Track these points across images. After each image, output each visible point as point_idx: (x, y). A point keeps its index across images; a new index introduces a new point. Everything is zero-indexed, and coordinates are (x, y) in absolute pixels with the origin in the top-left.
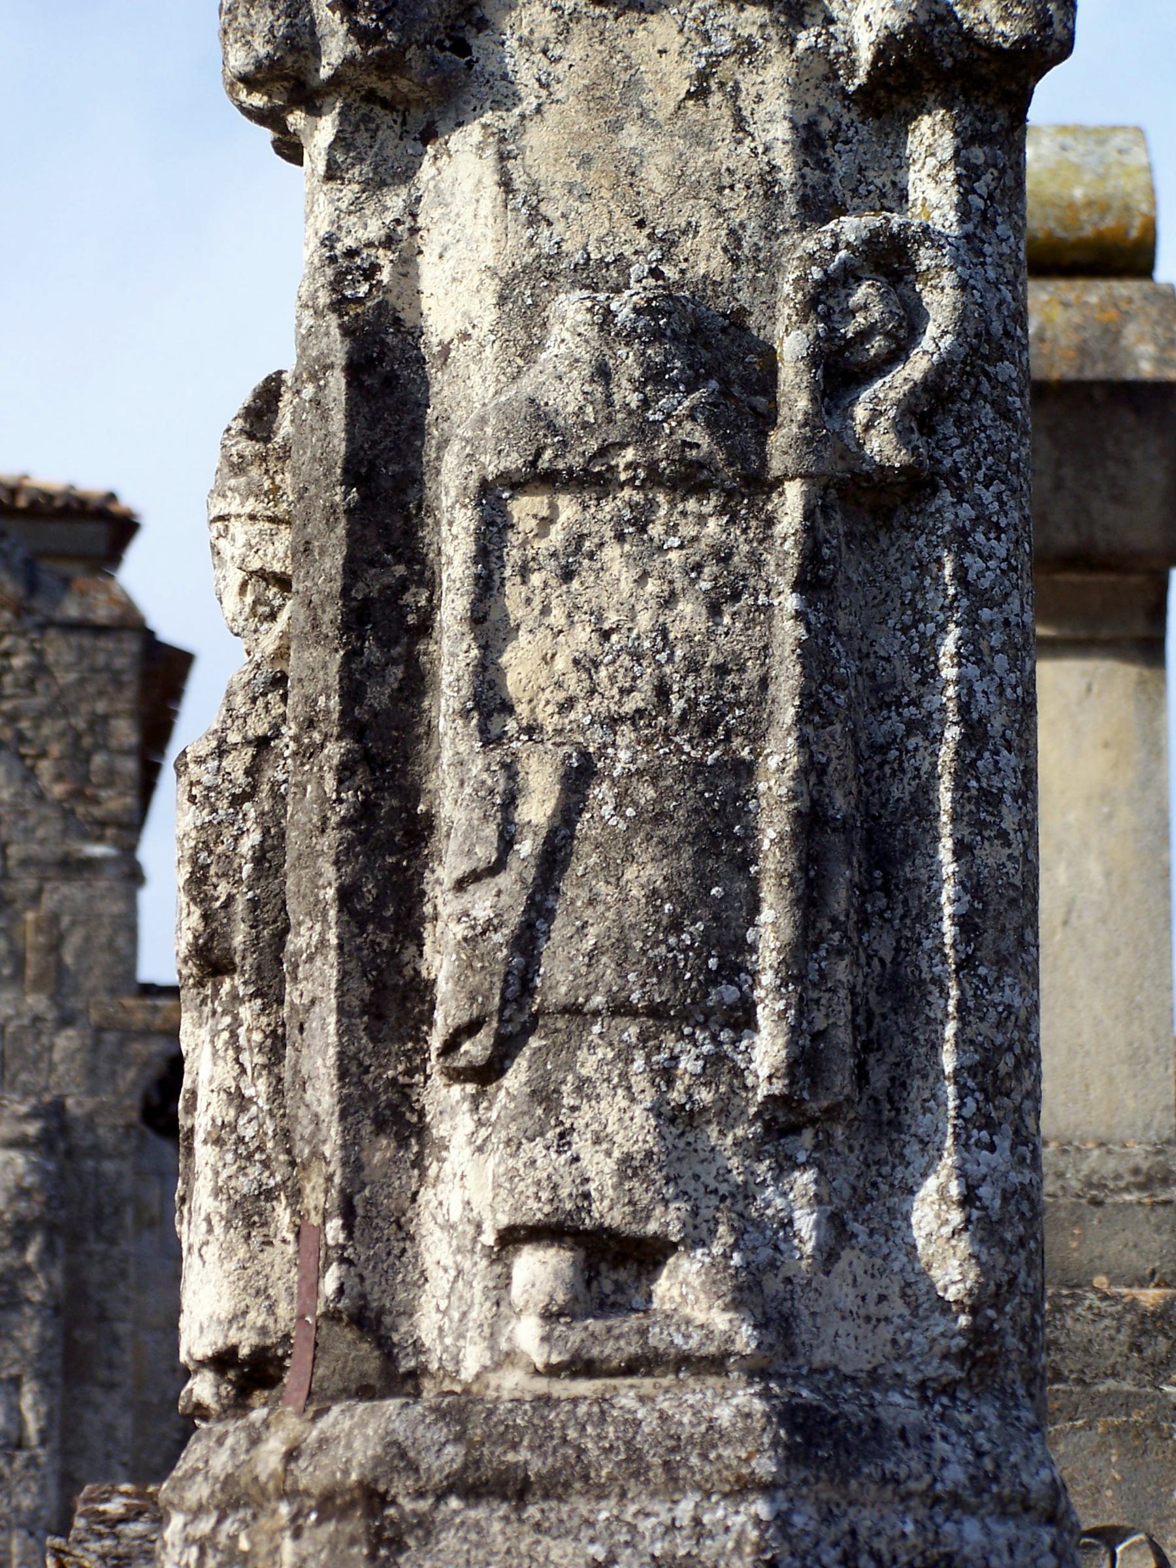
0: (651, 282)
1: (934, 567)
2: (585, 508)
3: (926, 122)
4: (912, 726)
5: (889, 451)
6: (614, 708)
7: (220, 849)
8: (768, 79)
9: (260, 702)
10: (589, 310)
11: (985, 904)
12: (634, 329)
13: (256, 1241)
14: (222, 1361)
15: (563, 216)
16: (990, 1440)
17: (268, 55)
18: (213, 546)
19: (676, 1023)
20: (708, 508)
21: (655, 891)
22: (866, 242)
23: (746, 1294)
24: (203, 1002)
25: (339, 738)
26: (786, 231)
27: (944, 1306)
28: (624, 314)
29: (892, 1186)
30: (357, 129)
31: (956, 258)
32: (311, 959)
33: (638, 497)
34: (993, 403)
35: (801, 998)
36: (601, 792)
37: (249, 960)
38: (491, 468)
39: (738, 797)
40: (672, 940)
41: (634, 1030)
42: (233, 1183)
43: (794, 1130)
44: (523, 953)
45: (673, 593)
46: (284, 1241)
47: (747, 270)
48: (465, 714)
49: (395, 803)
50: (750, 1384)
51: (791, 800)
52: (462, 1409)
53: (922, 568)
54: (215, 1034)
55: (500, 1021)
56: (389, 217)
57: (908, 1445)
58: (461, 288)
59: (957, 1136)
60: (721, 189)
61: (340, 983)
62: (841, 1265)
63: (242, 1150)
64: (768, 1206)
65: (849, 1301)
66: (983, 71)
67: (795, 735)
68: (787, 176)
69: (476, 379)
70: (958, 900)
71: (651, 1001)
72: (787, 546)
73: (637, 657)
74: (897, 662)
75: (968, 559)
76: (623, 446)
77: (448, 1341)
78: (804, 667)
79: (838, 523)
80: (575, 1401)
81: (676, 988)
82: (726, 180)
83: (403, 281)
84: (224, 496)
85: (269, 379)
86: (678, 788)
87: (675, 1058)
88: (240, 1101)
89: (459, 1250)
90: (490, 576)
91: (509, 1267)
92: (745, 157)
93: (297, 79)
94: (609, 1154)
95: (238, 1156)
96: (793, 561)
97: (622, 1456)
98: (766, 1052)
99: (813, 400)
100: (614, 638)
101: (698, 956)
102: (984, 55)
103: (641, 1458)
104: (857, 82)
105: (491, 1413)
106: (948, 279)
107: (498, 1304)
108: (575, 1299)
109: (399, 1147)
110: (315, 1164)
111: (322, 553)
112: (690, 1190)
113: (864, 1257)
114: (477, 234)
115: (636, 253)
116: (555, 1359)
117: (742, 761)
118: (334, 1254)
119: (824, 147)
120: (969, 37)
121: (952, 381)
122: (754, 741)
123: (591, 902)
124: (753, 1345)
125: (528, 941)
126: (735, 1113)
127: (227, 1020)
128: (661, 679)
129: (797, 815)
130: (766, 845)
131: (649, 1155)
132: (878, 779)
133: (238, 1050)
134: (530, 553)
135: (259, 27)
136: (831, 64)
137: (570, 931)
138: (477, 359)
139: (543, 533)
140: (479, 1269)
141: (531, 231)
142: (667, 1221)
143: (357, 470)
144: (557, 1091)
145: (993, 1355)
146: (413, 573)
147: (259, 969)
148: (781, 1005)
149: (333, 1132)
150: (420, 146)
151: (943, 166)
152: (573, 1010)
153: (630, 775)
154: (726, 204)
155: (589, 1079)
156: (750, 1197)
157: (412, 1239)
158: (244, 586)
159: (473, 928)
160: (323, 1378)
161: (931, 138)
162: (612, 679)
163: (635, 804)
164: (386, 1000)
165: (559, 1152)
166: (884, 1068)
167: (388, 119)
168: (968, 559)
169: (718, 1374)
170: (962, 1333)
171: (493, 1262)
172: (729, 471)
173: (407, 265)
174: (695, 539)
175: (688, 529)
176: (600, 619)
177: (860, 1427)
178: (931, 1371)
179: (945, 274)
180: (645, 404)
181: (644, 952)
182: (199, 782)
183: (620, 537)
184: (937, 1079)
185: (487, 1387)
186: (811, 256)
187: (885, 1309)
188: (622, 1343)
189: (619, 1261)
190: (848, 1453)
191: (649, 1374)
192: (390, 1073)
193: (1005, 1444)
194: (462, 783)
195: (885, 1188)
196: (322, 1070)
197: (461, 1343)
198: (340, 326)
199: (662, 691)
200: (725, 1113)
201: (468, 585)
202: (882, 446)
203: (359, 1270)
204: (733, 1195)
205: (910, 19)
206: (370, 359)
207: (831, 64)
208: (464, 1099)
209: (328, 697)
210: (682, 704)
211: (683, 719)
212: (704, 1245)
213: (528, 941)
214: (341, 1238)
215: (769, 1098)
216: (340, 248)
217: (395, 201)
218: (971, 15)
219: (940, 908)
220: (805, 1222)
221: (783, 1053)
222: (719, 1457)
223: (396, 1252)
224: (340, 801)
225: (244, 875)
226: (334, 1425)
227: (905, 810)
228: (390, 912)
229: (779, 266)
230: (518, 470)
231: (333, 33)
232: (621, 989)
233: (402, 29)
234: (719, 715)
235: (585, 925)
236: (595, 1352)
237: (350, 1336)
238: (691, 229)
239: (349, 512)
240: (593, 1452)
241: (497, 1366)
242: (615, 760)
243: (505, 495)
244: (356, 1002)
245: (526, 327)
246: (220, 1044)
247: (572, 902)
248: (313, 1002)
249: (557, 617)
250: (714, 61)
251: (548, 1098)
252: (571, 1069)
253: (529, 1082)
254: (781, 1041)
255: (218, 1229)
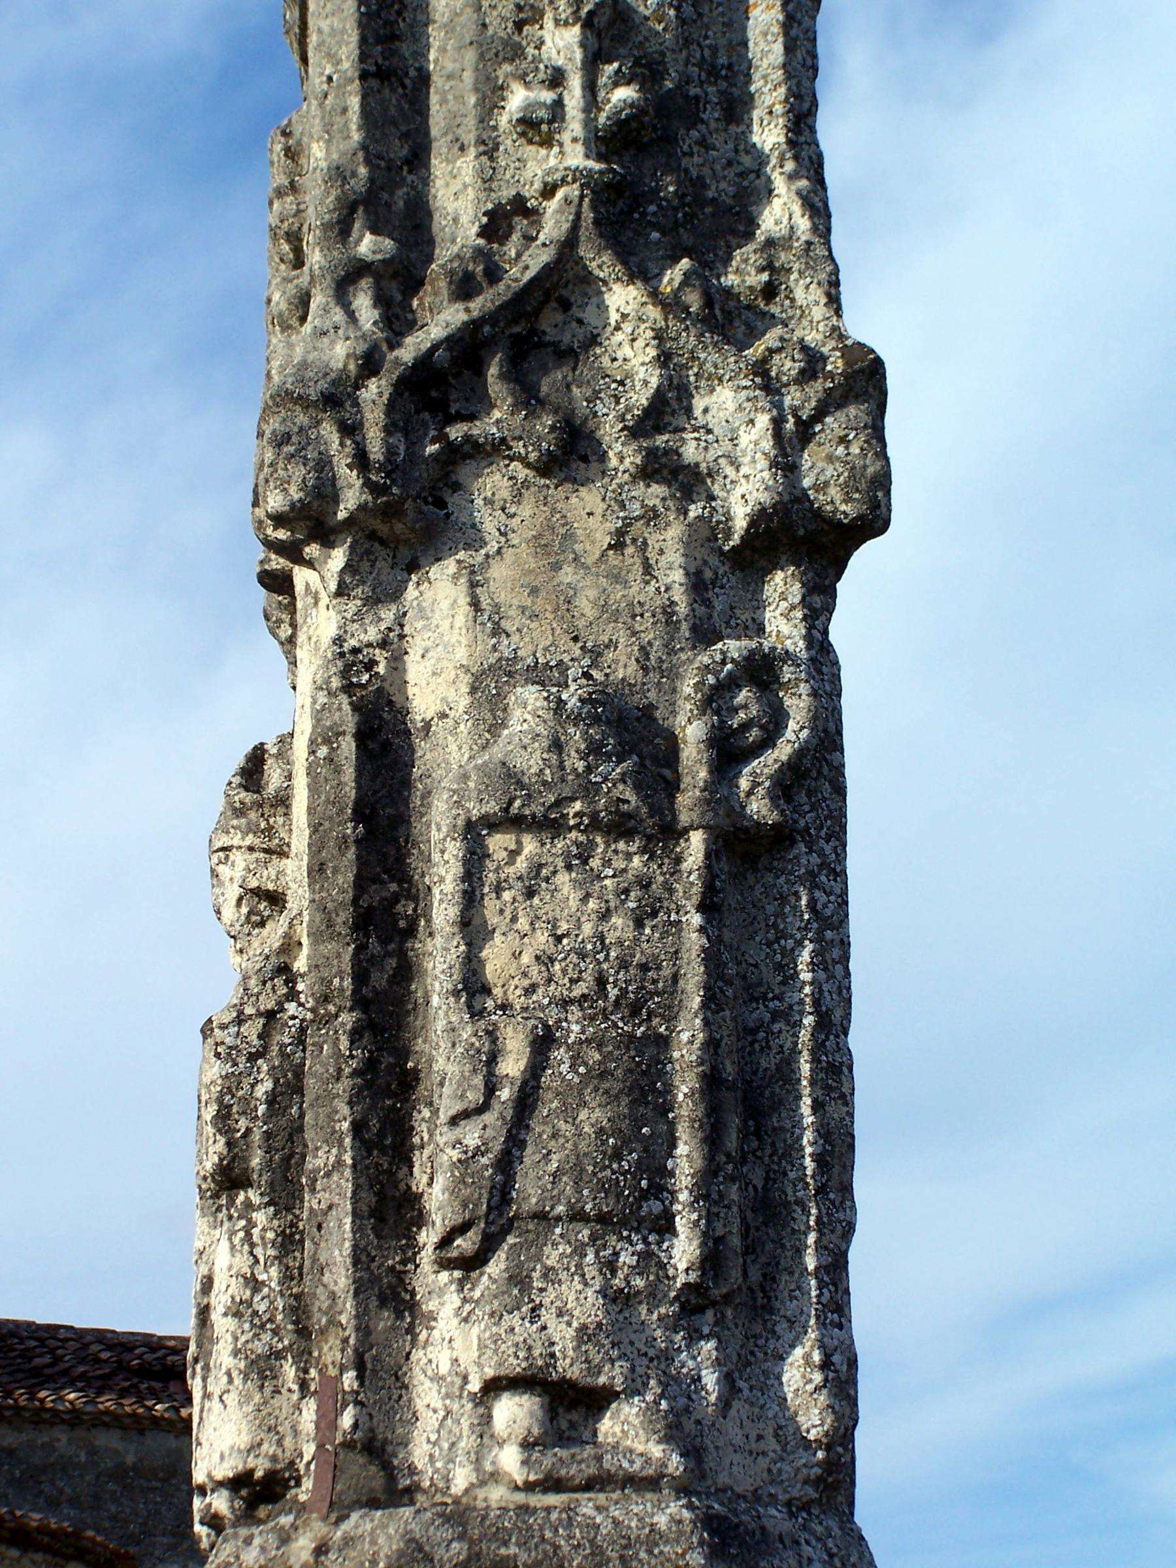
0: (584, 681)
1: (792, 899)
2: (543, 844)
3: (779, 576)
4: (776, 1015)
5: (764, 812)
6: (565, 993)
7: (241, 1093)
8: (668, 538)
9: (269, 985)
10: (546, 699)
11: (833, 1146)
12: (580, 714)
13: (268, 1390)
14: (238, 1483)
15: (518, 630)
16: (836, 1545)
17: (300, 500)
18: (212, 871)
19: (617, 1228)
20: (633, 848)
21: (602, 1129)
22: (746, 659)
23: (674, 1431)
24: (219, 1209)
25: (351, 1010)
26: (682, 649)
27: (806, 1444)
28: (572, 703)
29: (766, 1354)
30: (361, 559)
31: (809, 673)
32: (328, 1175)
33: (582, 838)
34: (830, 782)
35: (708, 1211)
36: (559, 1054)
37: (264, 1178)
38: (475, 812)
39: (659, 1062)
40: (615, 1166)
41: (586, 1232)
42: (250, 1346)
43: (700, 1310)
44: (503, 1173)
45: (608, 910)
46: (290, 1390)
47: (654, 677)
48: (456, 993)
49: (391, 1060)
50: (678, 1499)
51: (699, 1065)
52: (462, 1515)
53: (783, 899)
54: (232, 1233)
55: (486, 1223)
56: (383, 626)
57: (785, 1547)
58: (440, 680)
59: (818, 1317)
60: (634, 616)
61: (354, 1193)
62: (733, 1412)
63: (256, 1321)
64: (682, 1367)
65: (738, 1440)
66: (824, 540)
67: (701, 1017)
68: (682, 609)
69: (453, 747)
70: (815, 1143)
71: (600, 1210)
72: (692, 878)
73: (582, 955)
74: (763, 968)
75: (817, 894)
76: (573, 799)
77: (439, 1465)
78: (706, 967)
79: (724, 865)
80: (548, 1510)
81: (618, 1202)
82: (638, 610)
83: (395, 673)
84: (228, 833)
85: (255, 748)
86: (616, 1053)
87: (616, 1254)
88: (254, 1284)
89: (447, 1396)
90: (473, 891)
91: (489, 1409)
92: (652, 594)
93: (317, 520)
94: (569, 1324)
95: (253, 1326)
96: (697, 890)
97: (588, 1551)
98: (683, 1251)
99: (711, 772)
100: (565, 941)
101: (634, 1178)
102: (826, 527)
103: (602, 1553)
104: (731, 543)
105: (484, 1518)
106: (804, 688)
107: (481, 1437)
108: (546, 1433)
109: (397, 1318)
110: (332, 1329)
111: (335, 871)
112: (628, 1353)
113: (747, 1406)
114: (453, 640)
115: (572, 660)
116: (532, 1478)
117: (661, 1035)
118: (350, 1398)
119: (707, 590)
120: (818, 514)
121: (807, 763)
122: (668, 1021)
123: (554, 1136)
124: (681, 1469)
125: (507, 1163)
126: (660, 1296)
127: (243, 1223)
128: (601, 972)
129: (703, 1077)
130: (681, 1097)
131: (599, 1325)
132: (750, 1054)
133: (252, 1245)
134: (503, 876)
135: (295, 478)
136: (713, 529)
137: (538, 1157)
138: (454, 732)
139: (511, 861)
140: (466, 1413)
141: (494, 641)
142: (613, 1375)
143: (363, 812)
144: (529, 1277)
145: (839, 1481)
146: (402, 889)
147: (272, 1184)
148: (695, 1216)
149: (348, 1305)
150: (405, 575)
151: (793, 607)
152: (541, 1216)
153: (581, 1042)
154: (637, 627)
155: (553, 1268)
156: (670, 1360)
157: (407, 1388)
158: (240, 900)
159: (466, 1152)
160: (341, 1493)
161: (782, 588)
162: (564, 971)
163: (586, 1064)
164: (389, 1210)
165: (532, 1323)
166: (758, 1266)
167: (383, 553)
168: (817, 894)
169: (654, 1491)
170: (819, 1464)
171: (476, 1405)
172: (650, 822)
173: (397, 661)
174: (624, 871)
175: (619, 864)
176: (555, 927)
177: (754, 1533)
178: (795, 1493)
179: (802, 685)
180: (589, 769)
181: (594, 1174)
182: (223, 1043)
183: (569, 867)
184: (801, 1274)
185: (475, 1499)
186: (707, 667)
187: (762, 1445)
188: (583, 1466)
189: (572, 1406)
190: (749, 1552)
191: (601, 1490)
192: (390, 1262)
193: (846, 1548)
194: (454, 1045)
195: (760, 1355)
196: (339, 1259)
197: (451, 1466)
198: (351, 704)
199: (601, 981)
200: (653, 1295)
201: (458, 898)
202: (759, 808)
203: (369, 1410)
204: (658, 1358)
205: (777, 498)
206: (372, 728)
207: (713, 529)
208: (451, 1282)
209: (342, 979)
210: (616, 991)
211: (617, 1002)
212: (639, 1394)
213: (507, 1163)
214: (356, 1386)
215: (686, 1285)
216: (347, 647)
217: (388, 615)
218: (821, 498)
219: (802, 1149)
220: (710, 1379)
221: (698, 1252)
222: (661, 1552)
223: (395, 1397)
224: (352, 1057)
225: (260, 1113)
226: (356, 1527)
227: (772, 1077)
228: (388, 1142)
229: (677, 675)
230: (495, 814)
231: (350, 486)
232: (578, 1201)
233: (402, 486)
234: (643, 999)
235: (549, 1153)
236: (563, 1472)
237: (361, 1461)
238: (612, 644)
239: (357, 842)
240: (566, 1549)
241: (482, 1483)
242: (569, 1031)
243: (484, 832)
244: (365, 1208)
245: (491, 710)
246: (236, 1240)
247: (540, 1135)
248: (330, 1207)
249: (523, 924)
250: (628, 522)
251: (522, 1282)
252: (539, 1260)
253: (507, 1270)
254: (696, 1243)
255: (238, 1381)
